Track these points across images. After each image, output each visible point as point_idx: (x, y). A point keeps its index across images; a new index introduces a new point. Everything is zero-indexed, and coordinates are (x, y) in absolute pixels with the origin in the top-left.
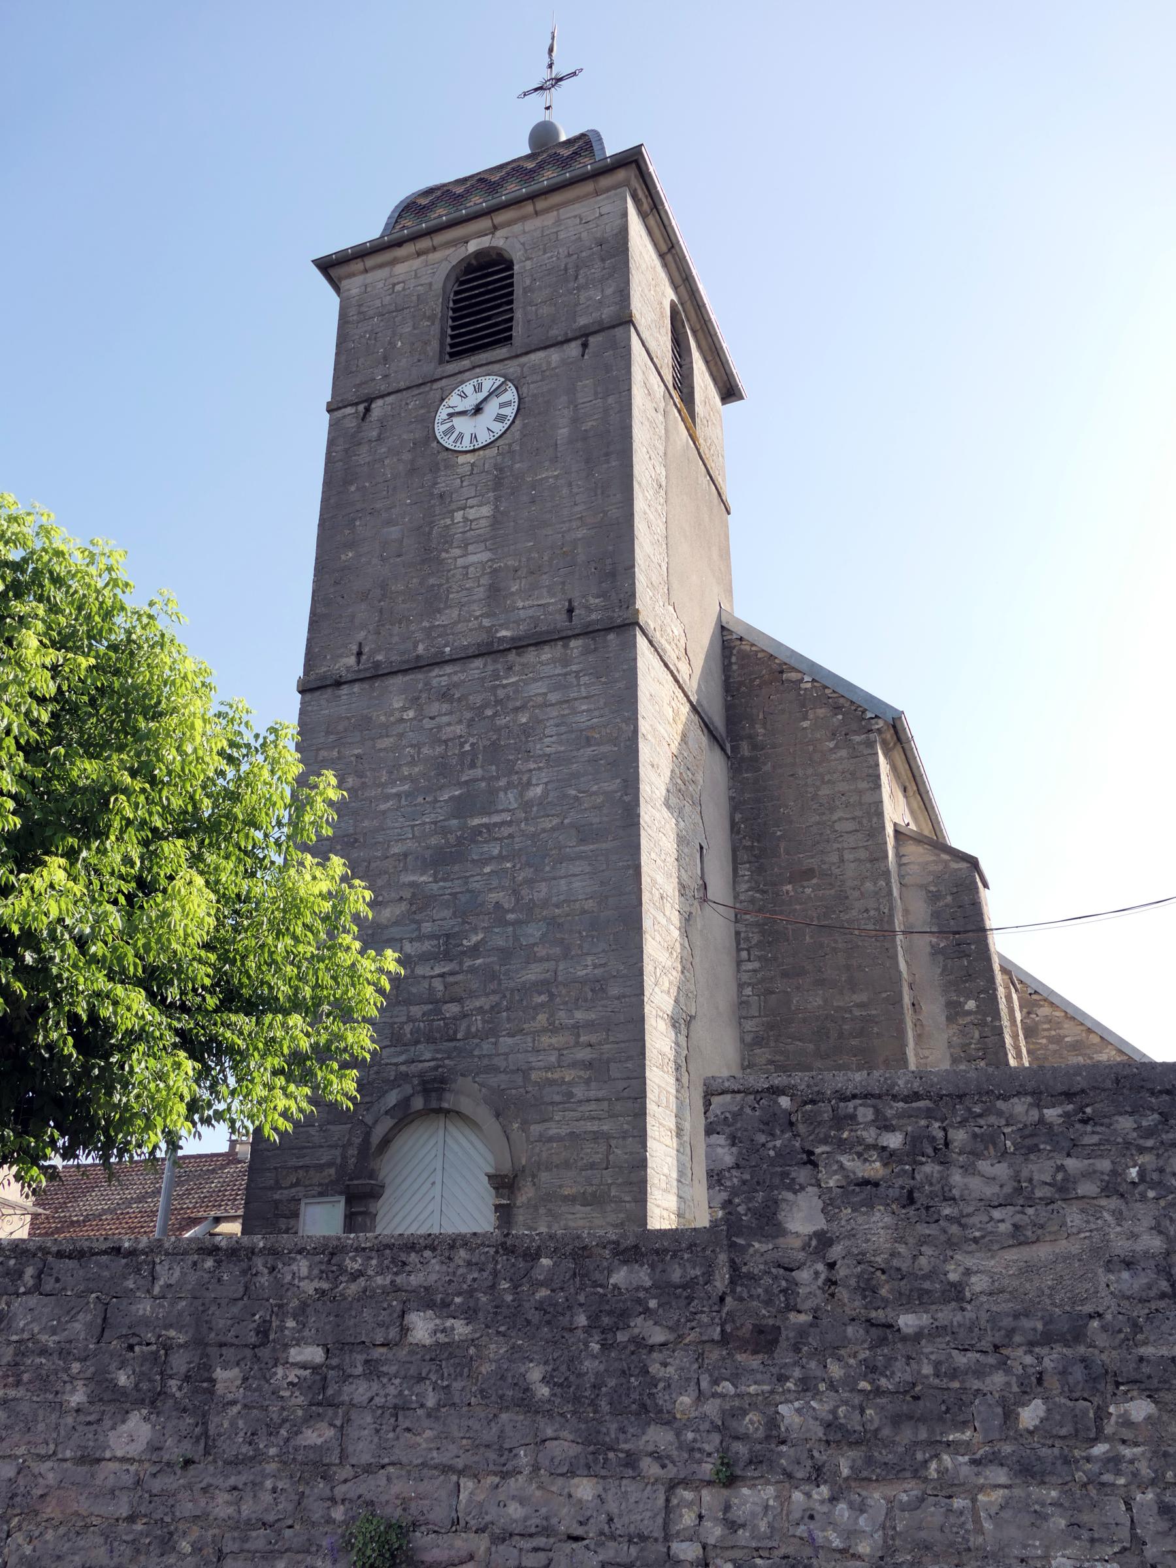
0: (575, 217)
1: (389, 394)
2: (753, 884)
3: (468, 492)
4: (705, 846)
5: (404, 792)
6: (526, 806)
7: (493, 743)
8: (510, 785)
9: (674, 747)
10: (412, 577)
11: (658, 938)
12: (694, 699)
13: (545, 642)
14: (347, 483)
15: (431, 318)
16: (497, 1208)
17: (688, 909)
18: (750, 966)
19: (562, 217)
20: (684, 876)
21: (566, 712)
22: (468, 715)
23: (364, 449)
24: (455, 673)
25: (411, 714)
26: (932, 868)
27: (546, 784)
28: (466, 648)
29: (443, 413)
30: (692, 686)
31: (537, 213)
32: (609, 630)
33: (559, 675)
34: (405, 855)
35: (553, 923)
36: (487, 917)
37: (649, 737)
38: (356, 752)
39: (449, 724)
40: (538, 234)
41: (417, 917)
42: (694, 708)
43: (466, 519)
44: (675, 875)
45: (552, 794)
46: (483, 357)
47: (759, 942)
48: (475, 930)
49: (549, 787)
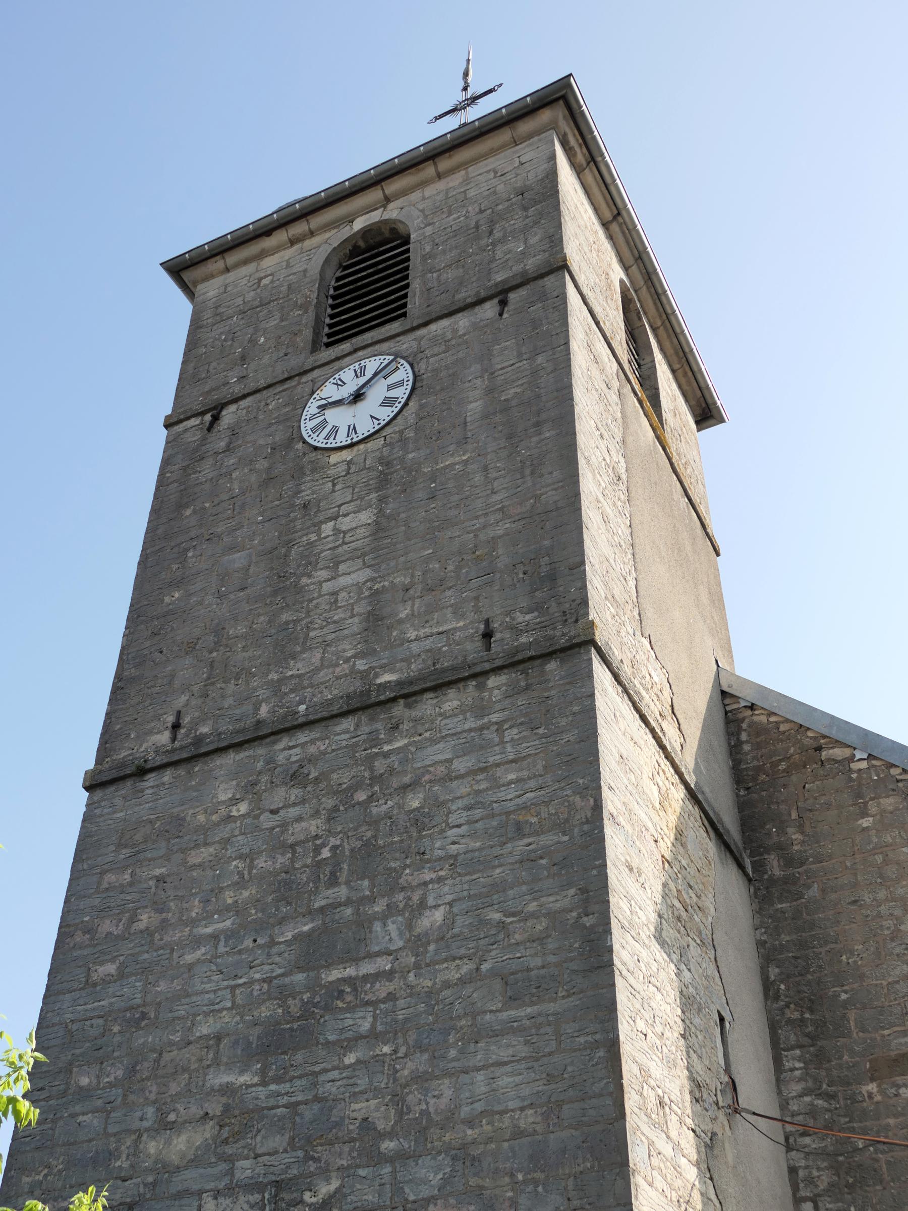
0: (489, 171)
1: (244, 397)
2: (810, 1084)
3: (341, 496)
4: (727, 1017)
5: (223, 931)
6: (417, 943)
7: (366, 844)
8: (391, 910)
9: (666, 846)
10: (259, 615)
11: (659, 1183)
12: (691, 779)
14: (180, 506)
15: (304, 307)
17: (708, 1127)
19: (470, 176)
20: (698, 1067)
21: (483, 786)
22: (329, 803)
23: (208, 463)
24: (313, 742)
25: (243, 808)
27: (450, 904)
28: (330, 703)
29: (312, 407)
30: (688, 761)
31: (439, 176)
33: (470, 730)
34: (218, 1038)
35: (462, 1155)
36: (346, 1148)
37: (621, 819)
38: (158, 872)
39: (299, 819)
40: (441, 197)
41: (229, 1150)
42: (692, 795)
43: (337, 531)
44: (682, 1064)
45: (459, 921)
46: (368, 337)
47: (832, 1185)
48: (325, 1173)
49: (455, 910)
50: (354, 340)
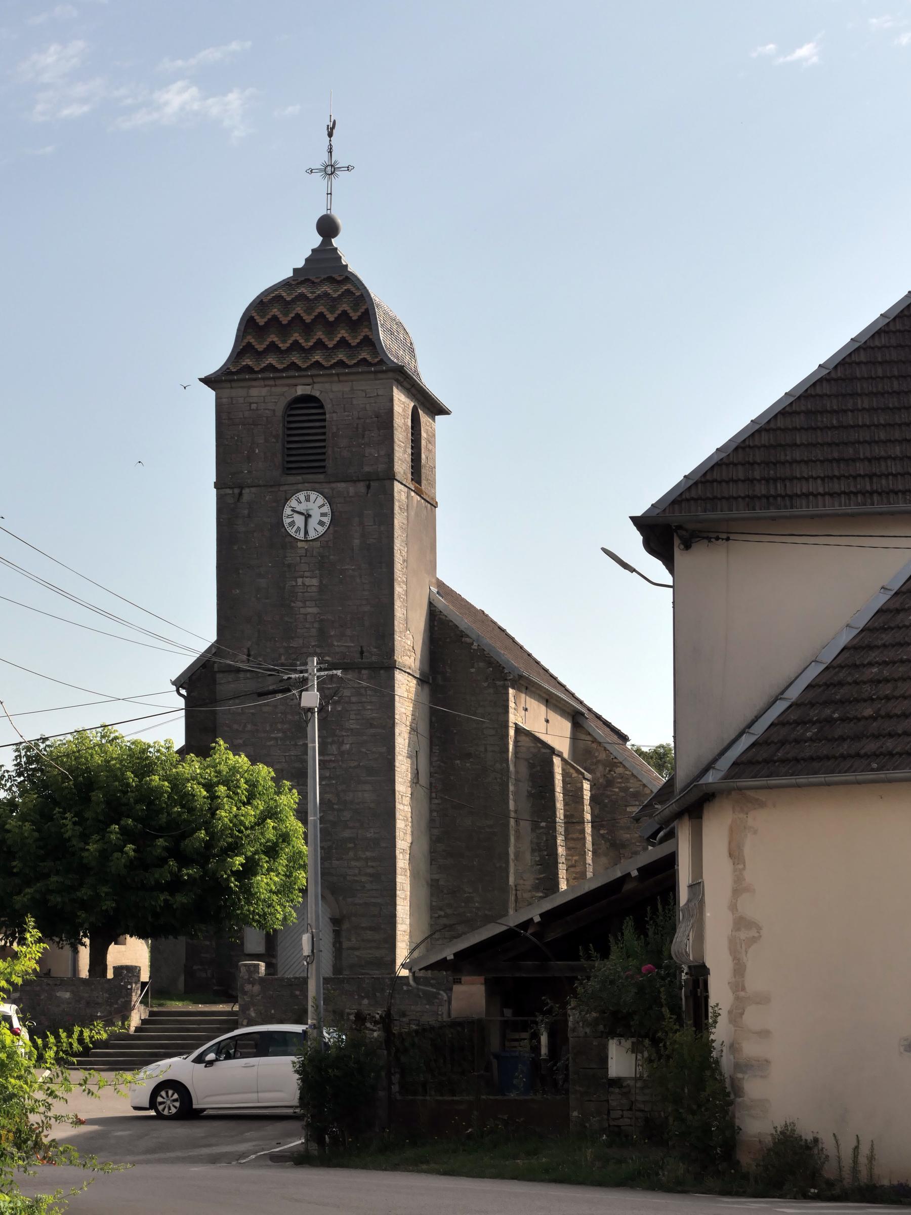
6: (342, 753)
13: (351, 669)
16: (334, 931)
18: (436, 801)
26: (533, 750)
32: (381, 668)
50: (305, 476)
